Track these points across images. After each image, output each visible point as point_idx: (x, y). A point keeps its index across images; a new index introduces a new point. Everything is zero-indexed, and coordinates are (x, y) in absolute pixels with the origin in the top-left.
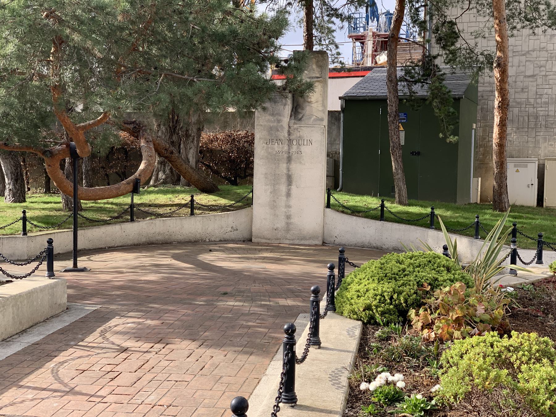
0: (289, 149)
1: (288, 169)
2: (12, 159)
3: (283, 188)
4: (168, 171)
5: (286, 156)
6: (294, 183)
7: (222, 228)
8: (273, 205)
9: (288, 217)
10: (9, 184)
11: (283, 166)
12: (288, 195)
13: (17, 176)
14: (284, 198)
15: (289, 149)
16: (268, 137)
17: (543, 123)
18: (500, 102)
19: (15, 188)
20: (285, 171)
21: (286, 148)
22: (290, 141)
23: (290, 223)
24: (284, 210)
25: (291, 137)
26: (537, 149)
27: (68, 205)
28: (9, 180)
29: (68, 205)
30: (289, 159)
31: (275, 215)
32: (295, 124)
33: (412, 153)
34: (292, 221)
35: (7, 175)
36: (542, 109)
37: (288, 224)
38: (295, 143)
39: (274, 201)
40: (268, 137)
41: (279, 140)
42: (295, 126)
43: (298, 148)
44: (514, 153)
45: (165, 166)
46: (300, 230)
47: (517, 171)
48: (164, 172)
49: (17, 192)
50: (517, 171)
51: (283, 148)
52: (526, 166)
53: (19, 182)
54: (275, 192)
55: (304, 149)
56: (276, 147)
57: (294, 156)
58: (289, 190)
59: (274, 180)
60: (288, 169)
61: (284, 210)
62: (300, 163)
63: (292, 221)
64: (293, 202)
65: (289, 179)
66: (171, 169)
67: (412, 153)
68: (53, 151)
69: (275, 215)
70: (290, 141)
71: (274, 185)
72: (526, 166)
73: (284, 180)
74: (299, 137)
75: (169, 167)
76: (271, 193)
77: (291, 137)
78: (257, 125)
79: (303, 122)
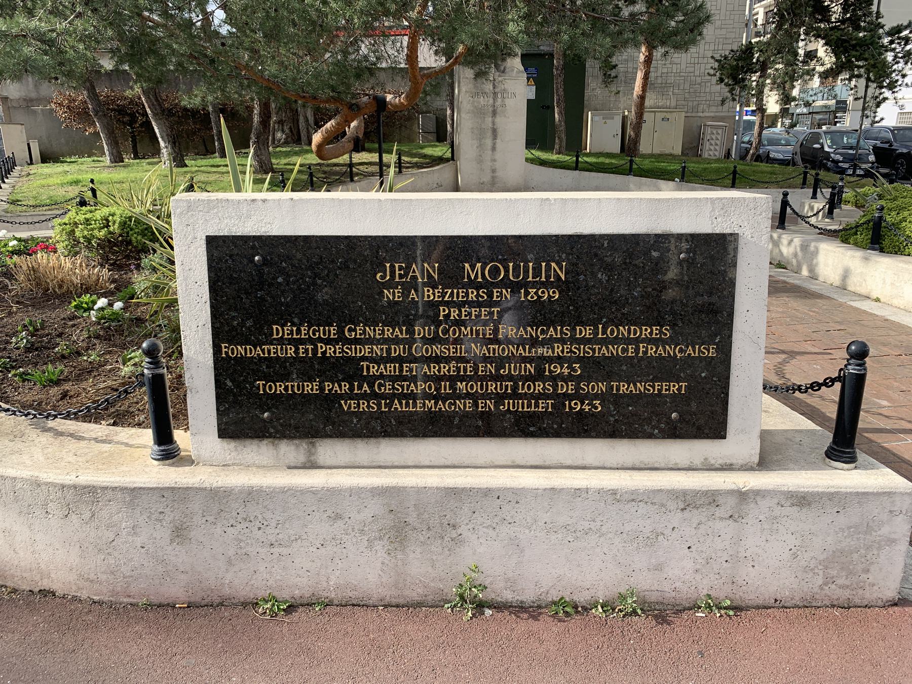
0: (494, 103)
1: (493, 123)
2: (166, 119)
3: (489, 142)
4: (287, 131)
5: (491, 109)
6: (499, 137)
7: (428, 184)
8: (480, 160)
9: (494, 171)
10: (166, 147)
11: (489, 120)
12: (494, 149)
13: (174, 138)
14: (490, 152)
15: (494, 103)
16: (474, 90)
17: (623, 79)
18: (646, 56)
19: (175, 152)
20: (490, 125)
21: (491, 101)
22: (495, 94)
23: (496, 177)
24: (490, 164)
25: (496, 90)
26: (617, 103)
27: (262, 167)
28: (165, 143)
29: (262, 167)
30: (494, 113)
31: (482, 170)
32: (499, 76)
33: (542, 107)
34: (497, 174)
35: (162, 137)
36: (623, 66)
37: (493, 178)
38: (499, 96)
39: (480, 156)
40: (474, 90)
41: (484, 93)
42: (500, 79)
43: (502, 101)
44: (598, 106)
45: (283, 125)
46: (505, 183)
47: (605, 123)
48: (283, 131)
49: (177, 156)
50: (605, 123)
51: (488, 101)
52: (613, 118)
53: (177, 144)
54: (481, 146)
55: (507, 101)
56: (482, 101)
57: (499, 110)
58: (494, 144)
59: (479, 134)
60: (493, 123)
61: (490, 164)
62: (505, 116)
63: (497, 174)
64: (498, 155)
65: (495, 132)
66: (290, 128)
67: (542, 107)
68: (360, 103)
69: (482, 170)
70: (495, 94)
71: (480, 140)
72: (613, 118)
73: (489, 134)
74: (504, 90)
75: (288, 127)
76: (477, 147)
77: (496, 90)
78: (463, 78)
79: (507, 75)
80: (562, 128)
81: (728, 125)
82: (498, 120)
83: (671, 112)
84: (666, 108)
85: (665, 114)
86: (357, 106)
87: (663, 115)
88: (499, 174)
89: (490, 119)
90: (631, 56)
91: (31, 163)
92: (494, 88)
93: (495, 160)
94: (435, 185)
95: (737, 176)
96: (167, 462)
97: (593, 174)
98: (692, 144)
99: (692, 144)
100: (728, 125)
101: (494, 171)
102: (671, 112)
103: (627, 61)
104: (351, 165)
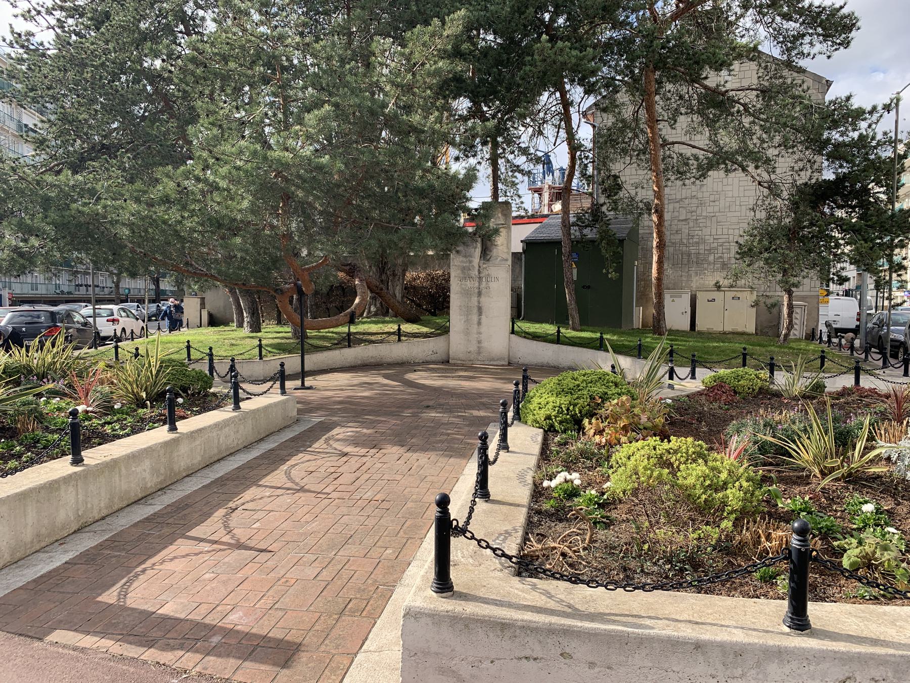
0: (479, 285)
1: (479, 302)
3: (475, 318)
4: (378, 305)
5: (476, 291)
6: (483, 314)
8: (467, 332)
9: (479, 342)
11: (475, 299)
12: (479, 323)
14: (476, 326)
15: (479, 285)
16: (462, 276)
17: (695, 260)
21: (477, 284)
30: (480, 294)
32: (484, 264)
33: (583, 287)
42: (484, 266)
47: (673, 301)
48: (375, 305)
54: (467, 321)
55: (491, 284)
57: (484, 291)
58: (480, 319)
59: (467, 311)
60: (479, 302)
62: (489, 296)
64: (483, 329)
65: (480, 309)
71: (467, 315)
73: (475, 310)
77: (481, 275)
80: (573, 306)
81: (806, 304)
82: (483, 299)
83: (741, 291)
84: (741, 287)
85: (735, 293)
86: (281, 290)
87: (733, 294)
88: (485, 344)
89: (476, 298)
90: (702, 239)
91: (201, 326)
92: (479, 273)
93: (480, 333)
94: (431, 352)
95: (119, 349)
96: (444, 595)
97: (576, 349)
98: (771, 322)
99: (771, 322)
100: (806, 304)
101: (479, 342)
102: (741, 291)
103: (698, 243)
104: (349, 334)
